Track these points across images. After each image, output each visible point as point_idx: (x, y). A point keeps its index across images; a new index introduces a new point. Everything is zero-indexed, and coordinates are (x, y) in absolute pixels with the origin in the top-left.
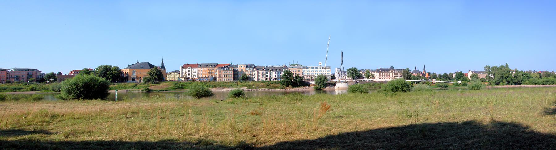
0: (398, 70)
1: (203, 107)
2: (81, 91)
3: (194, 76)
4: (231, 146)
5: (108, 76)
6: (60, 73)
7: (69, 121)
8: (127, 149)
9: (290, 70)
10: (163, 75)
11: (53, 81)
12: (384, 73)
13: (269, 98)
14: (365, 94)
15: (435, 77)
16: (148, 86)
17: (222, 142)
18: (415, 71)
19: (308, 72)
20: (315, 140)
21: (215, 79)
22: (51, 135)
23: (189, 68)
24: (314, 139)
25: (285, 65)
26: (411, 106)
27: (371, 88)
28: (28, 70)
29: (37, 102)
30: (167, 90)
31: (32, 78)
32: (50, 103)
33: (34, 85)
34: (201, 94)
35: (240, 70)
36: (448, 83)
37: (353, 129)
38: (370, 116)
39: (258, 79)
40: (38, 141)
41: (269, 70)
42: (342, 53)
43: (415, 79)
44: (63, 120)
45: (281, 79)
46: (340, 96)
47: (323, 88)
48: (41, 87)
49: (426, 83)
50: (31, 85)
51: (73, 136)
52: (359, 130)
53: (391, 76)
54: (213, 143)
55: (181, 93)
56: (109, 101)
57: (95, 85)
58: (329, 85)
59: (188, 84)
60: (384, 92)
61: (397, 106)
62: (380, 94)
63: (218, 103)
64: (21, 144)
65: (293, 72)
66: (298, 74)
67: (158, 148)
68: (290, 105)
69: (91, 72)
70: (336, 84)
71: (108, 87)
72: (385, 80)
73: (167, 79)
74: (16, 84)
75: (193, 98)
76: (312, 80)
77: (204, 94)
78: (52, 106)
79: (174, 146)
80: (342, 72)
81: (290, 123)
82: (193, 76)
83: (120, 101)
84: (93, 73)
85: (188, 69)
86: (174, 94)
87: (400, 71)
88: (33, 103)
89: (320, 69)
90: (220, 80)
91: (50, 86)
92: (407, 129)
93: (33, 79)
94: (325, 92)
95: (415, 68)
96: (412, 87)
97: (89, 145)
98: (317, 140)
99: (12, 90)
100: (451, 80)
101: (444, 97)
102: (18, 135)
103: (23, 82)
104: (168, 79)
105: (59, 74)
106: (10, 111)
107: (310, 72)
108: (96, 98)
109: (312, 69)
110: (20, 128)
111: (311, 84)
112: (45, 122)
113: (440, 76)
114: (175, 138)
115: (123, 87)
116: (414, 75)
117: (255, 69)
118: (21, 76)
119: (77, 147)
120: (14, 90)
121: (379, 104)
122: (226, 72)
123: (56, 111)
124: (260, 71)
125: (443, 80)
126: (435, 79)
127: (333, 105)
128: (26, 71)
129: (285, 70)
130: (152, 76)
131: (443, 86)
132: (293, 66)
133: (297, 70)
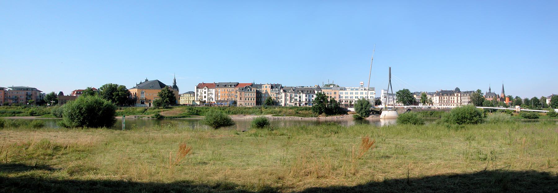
0: (465, 92)
1: (222, 140)
2: (84, 117)
3: (211, 99)
4: (255, 191)
5: (113, 98)
6: (61, 93)
7: (73, 155)
8: (137, 192)
9: (324, 92)
10: (175, 97)
11: (55, 104)
12: (445, 97)
13: (298, 129)
14: (420, 126)
15: (518, 102)
16: (159, 112)
17: (244, 186)
18: (489, 94)
19: (347, 95)
20: (353, 187)
21: (235, 103)
22: (54, 171)
23: (205, 89)
24: (353, 186)
25: (318, 86)
26: (484, 145)
27: (427, 118)
28: (27, 89)
29: (38, 130)
30: (180, 117)
31: (31, 99)
32: (51, 131)
33: (33, 108)
34: (219, 123)
35: (264, 92)
36: (538, 112)
37: (403, 174)
38: (243, 163)
39: (285, 104)
40: (41, 179)
41: (298, 91)
42: (390, 69)
43: (489, 105)
44: (66, 154)
45: (313, 104)
46: (388, 128)
47: (365, 117)
48: (41, 111)
49: (505, 112)
50: (31, 108)
51: (78, 173)
52: (411, 176)
53: (456, 102)
54: (234, 187)
55: (197, 120)
56: (116, 130)
57: (100, 109)
58: (373, 113)
59: (204, 110)
60: (446, 124)
61: (281, 150)
62: (440, 127)
63: (238, 134)
64: (23, 182)
65: (328, 95)
66: (333, 97)
67: (171, 191)
68: (141, 145)
69: (96, 92)
70: (381, 112)
71: (115, 112)
72: (447, 107)
73: (180, 102)
74: (14, 106)
75: (210, 128)
76: (351, 106)
77: (222, 123)
78: (54, 135)
79: (190, 189)
80: (390, 95)
81: (323, 163)
82: (210, 99)
83: (128, 130)
84: (98, 93)
85: (204, 89)
86: (188, 123)
87: (468, 95)
88: (34, 131)
89: (362, 91)
90: (241, 104)
91: (51, 110)
92: (480, 177)
93: (33, 100)
94: (368, 122)
95: (490, 90)
96: (485, 117)
97: (96, 186)
98: (356, 187)
99: (11, 114)
100: (543, 107)
101: (533, 133)
102: (19, 171)
103: (22, 104)
104: (181, 103)
105: (61, 95)
106: (8, 140)
107: (349, 95)
108: (102, 127)
109: (352, 91)
110: (21, 162)
111: (350, 111)
112: (47, 155)
113: (527, 101)
114: (190, 179)
115: (131, 113)
116: (488, 99)
117: (282, 91)
118: (19, 96)
119: (82, 187)
120: (13, 115)
121: (438, 141)
122: (247, 94)
123: (58, 141)
124: (288, 94)
125: (531, 108)
126: (520, 105)
127: (377, 140)
128: (25, 91)
129: (318, 92)
130: (163, 98)
131: (530, 116)
132: (328, 86)
133: (333, 92)
